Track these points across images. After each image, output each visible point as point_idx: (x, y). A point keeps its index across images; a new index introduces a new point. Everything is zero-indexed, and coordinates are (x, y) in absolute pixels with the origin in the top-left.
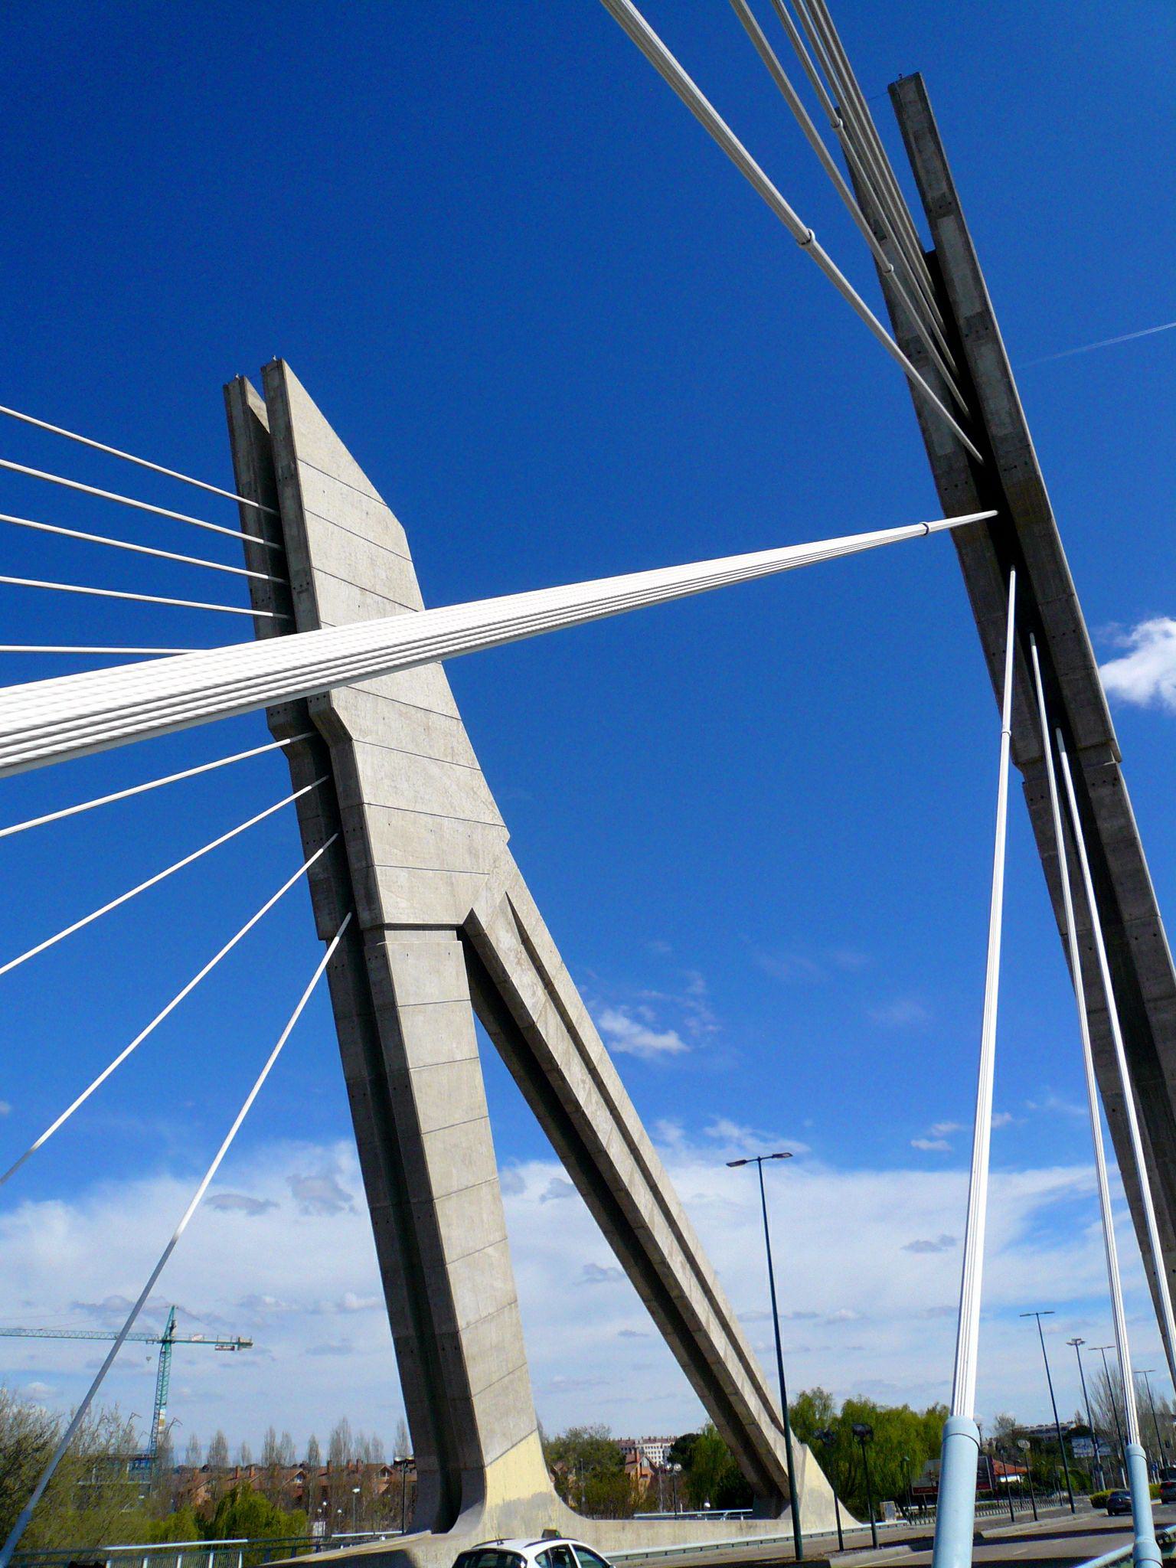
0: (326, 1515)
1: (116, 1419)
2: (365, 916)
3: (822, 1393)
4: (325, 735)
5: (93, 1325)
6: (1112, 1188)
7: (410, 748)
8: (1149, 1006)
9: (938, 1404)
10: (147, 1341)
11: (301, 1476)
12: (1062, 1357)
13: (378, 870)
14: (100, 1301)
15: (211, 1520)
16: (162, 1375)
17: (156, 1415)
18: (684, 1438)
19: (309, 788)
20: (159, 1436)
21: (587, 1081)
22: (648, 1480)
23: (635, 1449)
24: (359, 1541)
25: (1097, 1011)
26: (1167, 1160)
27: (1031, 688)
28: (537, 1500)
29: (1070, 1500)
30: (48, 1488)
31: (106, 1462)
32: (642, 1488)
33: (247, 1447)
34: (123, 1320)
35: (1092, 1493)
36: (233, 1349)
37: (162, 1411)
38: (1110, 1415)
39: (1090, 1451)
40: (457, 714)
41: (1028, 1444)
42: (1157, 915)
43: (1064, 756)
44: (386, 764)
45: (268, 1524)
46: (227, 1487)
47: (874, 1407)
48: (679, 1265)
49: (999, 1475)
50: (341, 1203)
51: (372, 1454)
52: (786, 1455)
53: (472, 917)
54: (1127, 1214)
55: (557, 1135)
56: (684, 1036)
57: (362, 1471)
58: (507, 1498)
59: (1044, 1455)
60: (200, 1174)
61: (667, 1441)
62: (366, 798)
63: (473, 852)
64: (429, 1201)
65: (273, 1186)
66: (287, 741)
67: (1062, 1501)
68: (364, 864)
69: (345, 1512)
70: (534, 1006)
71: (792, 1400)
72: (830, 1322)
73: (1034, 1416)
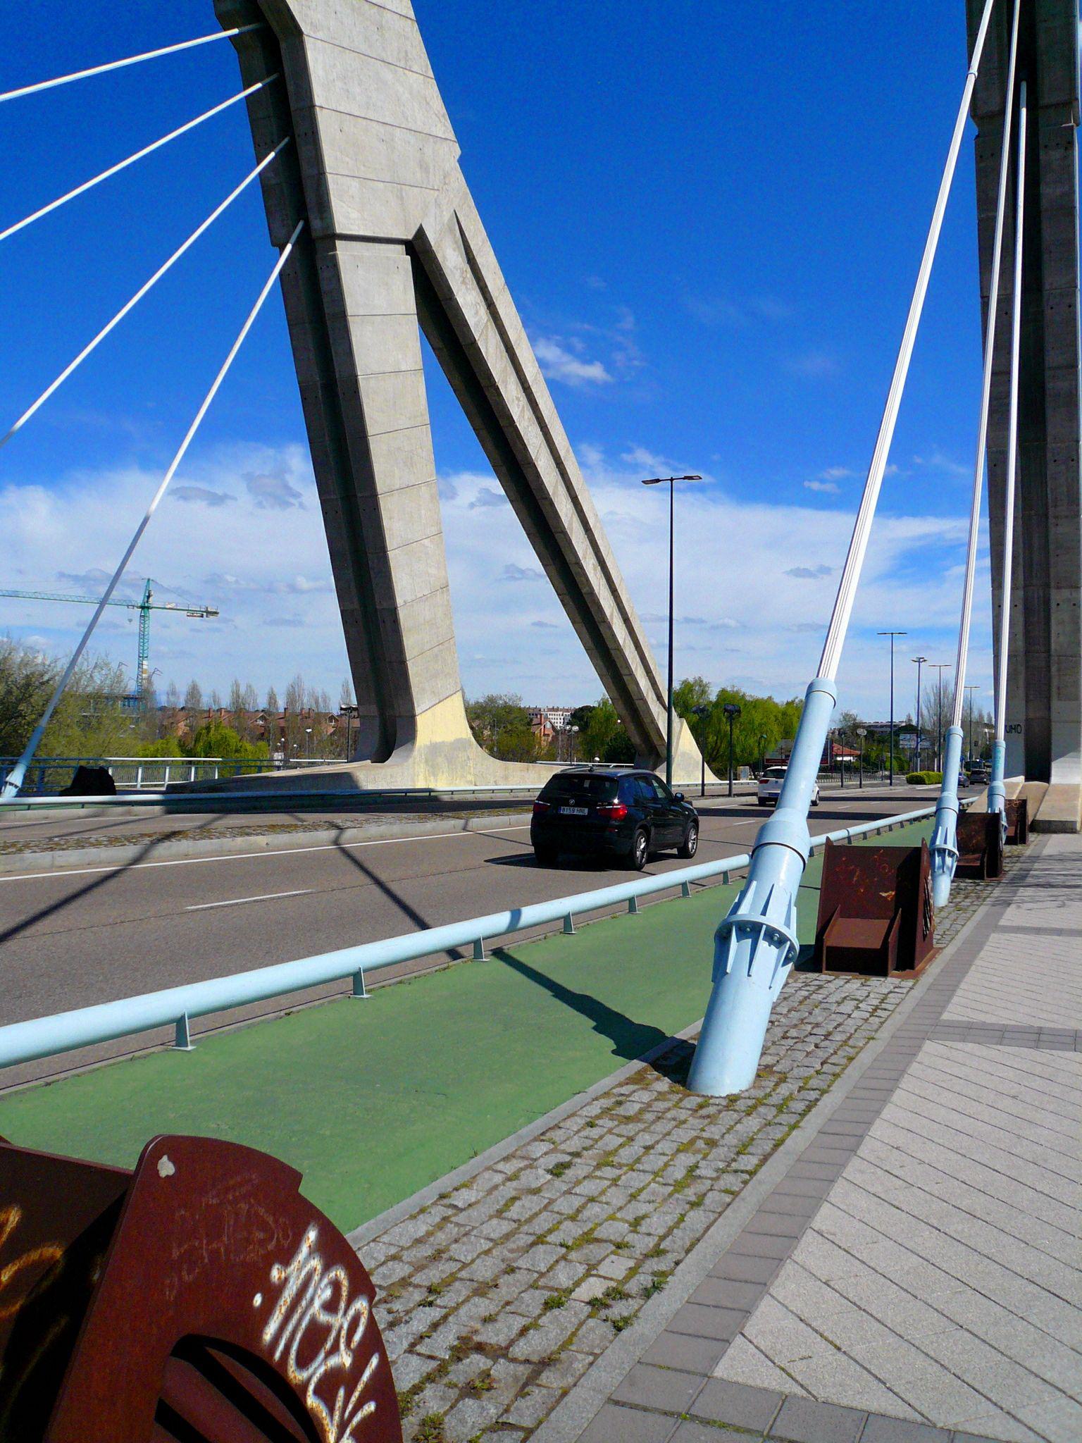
0: (284, 748)
1: (107, 664)
2: (316, 224)
3: (702, 681)
4: (274, 25)
5: (79, 591)
6: (980, 539)
7: (363, 48)
8: (1048, 373)
9: (797, 698)
10: (128, 606)
11: (263, 718)
12: (906, 670)
13: (330, 178)
14: (82, 573)
15: (192, 746)
16: (142, 635)
17: (140, 665)
18: (582, 709)
19: (259, 85)
20: (144, 681)
21: (522, 399)
22: (550, 738)
23: (541, 715)
24: (313, 764)
25: (1001, 374)
26: (1033, 512)
27: (1006, 35)
28: (459, 745)
29: (890, 778)
30: (55, 713)
31: (100, 699)
32: (545, 743)
33: (217, 694)
34: (103, 590)
35: (906, 774)
36: (202, 616)
37: (144, 662)
38: (935, 718)
39: (913, 744)
40: (412, 14)
41: (866, 732)
42: (1076, 287)
43: (1024, 111)
44: (338, 64)
45: (237, 751)
46: (203, 723)
47: (743, 696)
48: (591, 566)
49: (837, 755)
50: (292, 500)
51: (322, 705)
52: (666, 725)
53: (421, 233)
54: (988, 578)
55: (490, 445)
56: (609, 367)
57: (315, 717)
58: (433, 741)
59: (876, 744)
60: (166, 469)
61: (567, 711)
62: (318, 100)
63: (423, 166)
64: (373, 497)
65: (230, 481)
66: (235, 31)
67: (883, 777)
68: (316, 172)
69: (300, 746)
70: (477, 325)
71: (676, 686)
72: (713, 628)
73: (873, 713)
